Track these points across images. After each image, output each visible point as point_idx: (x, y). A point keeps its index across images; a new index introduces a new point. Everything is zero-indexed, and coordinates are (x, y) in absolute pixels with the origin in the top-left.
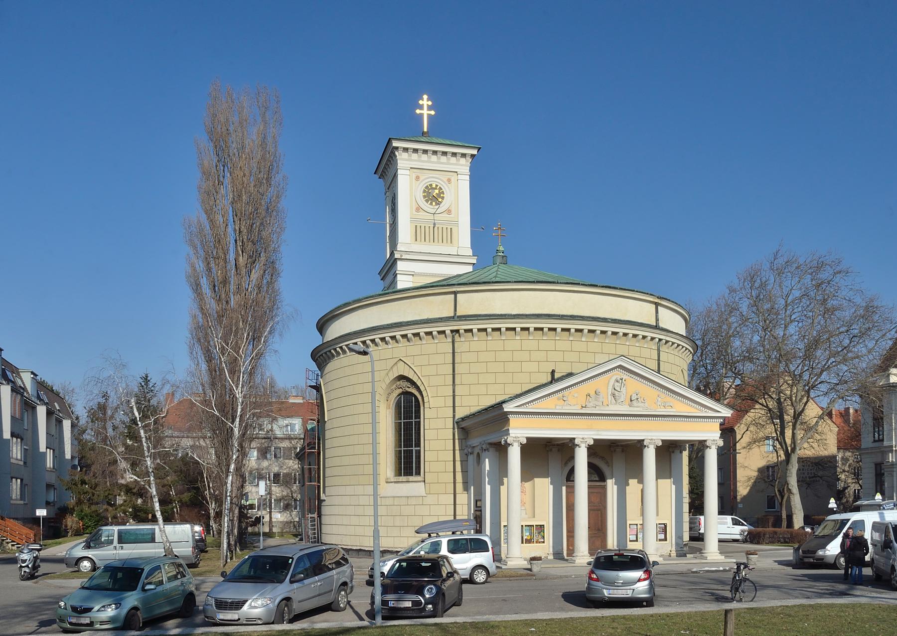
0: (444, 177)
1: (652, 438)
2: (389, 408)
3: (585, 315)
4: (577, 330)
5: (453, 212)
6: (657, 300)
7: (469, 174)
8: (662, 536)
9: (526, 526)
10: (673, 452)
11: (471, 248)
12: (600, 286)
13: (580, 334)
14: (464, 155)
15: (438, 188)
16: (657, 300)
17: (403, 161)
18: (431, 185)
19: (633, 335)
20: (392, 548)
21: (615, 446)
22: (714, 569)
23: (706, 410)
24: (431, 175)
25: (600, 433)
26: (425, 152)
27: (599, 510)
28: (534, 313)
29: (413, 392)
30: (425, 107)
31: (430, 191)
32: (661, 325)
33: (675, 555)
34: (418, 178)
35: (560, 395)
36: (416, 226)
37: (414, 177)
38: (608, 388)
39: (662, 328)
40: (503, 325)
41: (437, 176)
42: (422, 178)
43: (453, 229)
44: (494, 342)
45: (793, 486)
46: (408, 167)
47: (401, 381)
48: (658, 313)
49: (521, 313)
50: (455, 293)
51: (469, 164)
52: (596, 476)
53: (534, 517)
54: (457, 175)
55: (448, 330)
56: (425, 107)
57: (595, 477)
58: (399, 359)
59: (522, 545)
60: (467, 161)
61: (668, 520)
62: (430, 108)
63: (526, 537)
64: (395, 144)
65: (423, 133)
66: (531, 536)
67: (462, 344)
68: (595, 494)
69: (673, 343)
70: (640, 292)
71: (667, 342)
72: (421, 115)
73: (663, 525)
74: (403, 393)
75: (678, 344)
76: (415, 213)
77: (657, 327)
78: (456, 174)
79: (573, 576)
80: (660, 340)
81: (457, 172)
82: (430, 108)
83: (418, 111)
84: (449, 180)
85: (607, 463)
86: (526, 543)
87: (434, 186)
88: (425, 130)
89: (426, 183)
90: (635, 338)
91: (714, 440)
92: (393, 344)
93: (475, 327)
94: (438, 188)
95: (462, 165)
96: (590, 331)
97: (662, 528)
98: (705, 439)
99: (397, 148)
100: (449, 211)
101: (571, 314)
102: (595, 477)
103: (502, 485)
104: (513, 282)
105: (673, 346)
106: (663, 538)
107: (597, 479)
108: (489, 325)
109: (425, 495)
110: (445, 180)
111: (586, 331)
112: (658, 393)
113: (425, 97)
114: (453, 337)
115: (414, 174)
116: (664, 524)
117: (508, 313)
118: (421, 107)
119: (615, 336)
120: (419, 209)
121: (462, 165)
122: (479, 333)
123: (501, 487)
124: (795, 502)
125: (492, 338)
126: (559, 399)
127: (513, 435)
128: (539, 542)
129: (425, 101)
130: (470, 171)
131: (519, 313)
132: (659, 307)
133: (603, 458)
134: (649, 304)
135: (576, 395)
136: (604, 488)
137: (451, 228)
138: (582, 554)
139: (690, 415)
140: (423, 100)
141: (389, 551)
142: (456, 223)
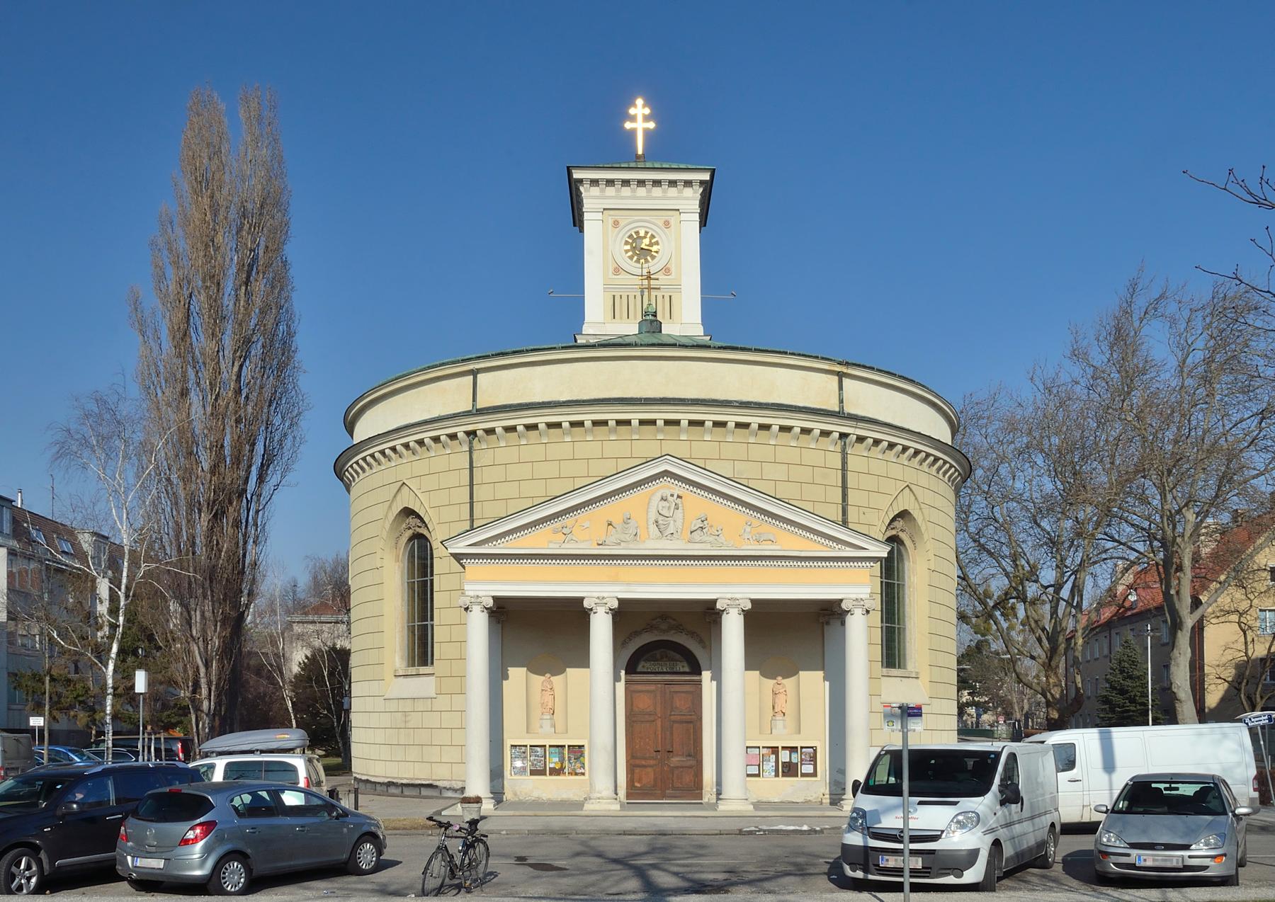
0: (659, 219)
1: (733, 596)
3: (688, 397)
4: (668, 423)
5: (673, 270)
6: (838, 368)
7: (699, 211)
8: (754, 770)
9: (550, 746)
10: (828, 623)
11: (702, 324)
12: (715, 348)
13: (699, 428)
14: (688, 183)
15: (649, 235)
16: (838, 368)
17: (592, 199)
18: (637, 233)
19: (780, 428)
20: (396, 778)
22: (792, 828)
23: (840, 546)
24: (636, 218)
25: (632, 588)
26: (626, 183)
27: (691, 722)
28: (597, 397)
29: (425, 533)
30: (640, 118)
31: (634, 245)
33: (828, 801)
34: (616, 223)
35: (557, 524)
36: (628, 296)
37: (611, 221)
38: (647, 511)
39: (849, 414)
40: (541, 419)
41: (647, 218)
42: (622, 224)
43: (673, 297)
44: (531, 448)
45: (1179, 687)
46: (601, 209)
47: (410, 518)
49: (575, 398)
50: (474, 373)
51: (699, 196)
52: (685, 664)
53: (799, 732)
54: (680, 213)
55: (460, 431)
56: (640, 118)
57: (683, 667)
58: (401, 483)
59: (777, 779)
60: (695, 192)
61: (820, 740)
62: (646, 118)
63: (552, 766)
64: (577, 175)
65: (638, 157)
66: (562, 764)
67: (485, 453)
68: (683, 695)
69: (905, 449)
70: (799, 355)
71: (861, 439)
72: (633, 133)
73: (812, 749)
74: (411, 539)
75: (903, 445)
76: (611, 276)
78: (678, 212)
79: (504, 832)
80: (843, 436)
81: (678, 210)
82: (647, 118)
83: (628, 125)
84: (667, 224)
85: (701, 641)
86: (783, 776)
87: (642, 234)
88: (640, 152)
89: (628, 231)
90: (809, 434)
94: (649, 235)
95: (687, 199)
96: (717, 424)
97: (810, 754)
98: (840, 598)
99: (581, 181)
100: (666, 270)
101: (662, 396)
102: (683, 667)
103: (617, 682)
104: (559, 349)
105: (907, 453)
106: (812, 771)
107: (687, 669)
108: (520, 421)
109: (435, 696)
110: (661, 223)
111: (684, 423)
113: (640, 102)
114: (471, 443)
115: (610, 217)
116: (812, 747)
117: (554, 399)
118: (633, 119)
119: (767, 432)
120: (618, 270)
121: (687, 199)
123: (504, 682)
124: (1183, 715)
125: (549, 439)
126: (555, 532)
127: (472, 594)
128: (576, 774)
129: (640, 109)
130: (699, 207)
131: (571, 399)
132: (843, 379)
133: (692, 634)
134: (824, 375)
135: (587, 524)
136: (699, 683)
137: (670, 297)
138: (599, 795)
139: (803, 554)
140: (635, 106)
141: (393, 782)
142: (677, 287)
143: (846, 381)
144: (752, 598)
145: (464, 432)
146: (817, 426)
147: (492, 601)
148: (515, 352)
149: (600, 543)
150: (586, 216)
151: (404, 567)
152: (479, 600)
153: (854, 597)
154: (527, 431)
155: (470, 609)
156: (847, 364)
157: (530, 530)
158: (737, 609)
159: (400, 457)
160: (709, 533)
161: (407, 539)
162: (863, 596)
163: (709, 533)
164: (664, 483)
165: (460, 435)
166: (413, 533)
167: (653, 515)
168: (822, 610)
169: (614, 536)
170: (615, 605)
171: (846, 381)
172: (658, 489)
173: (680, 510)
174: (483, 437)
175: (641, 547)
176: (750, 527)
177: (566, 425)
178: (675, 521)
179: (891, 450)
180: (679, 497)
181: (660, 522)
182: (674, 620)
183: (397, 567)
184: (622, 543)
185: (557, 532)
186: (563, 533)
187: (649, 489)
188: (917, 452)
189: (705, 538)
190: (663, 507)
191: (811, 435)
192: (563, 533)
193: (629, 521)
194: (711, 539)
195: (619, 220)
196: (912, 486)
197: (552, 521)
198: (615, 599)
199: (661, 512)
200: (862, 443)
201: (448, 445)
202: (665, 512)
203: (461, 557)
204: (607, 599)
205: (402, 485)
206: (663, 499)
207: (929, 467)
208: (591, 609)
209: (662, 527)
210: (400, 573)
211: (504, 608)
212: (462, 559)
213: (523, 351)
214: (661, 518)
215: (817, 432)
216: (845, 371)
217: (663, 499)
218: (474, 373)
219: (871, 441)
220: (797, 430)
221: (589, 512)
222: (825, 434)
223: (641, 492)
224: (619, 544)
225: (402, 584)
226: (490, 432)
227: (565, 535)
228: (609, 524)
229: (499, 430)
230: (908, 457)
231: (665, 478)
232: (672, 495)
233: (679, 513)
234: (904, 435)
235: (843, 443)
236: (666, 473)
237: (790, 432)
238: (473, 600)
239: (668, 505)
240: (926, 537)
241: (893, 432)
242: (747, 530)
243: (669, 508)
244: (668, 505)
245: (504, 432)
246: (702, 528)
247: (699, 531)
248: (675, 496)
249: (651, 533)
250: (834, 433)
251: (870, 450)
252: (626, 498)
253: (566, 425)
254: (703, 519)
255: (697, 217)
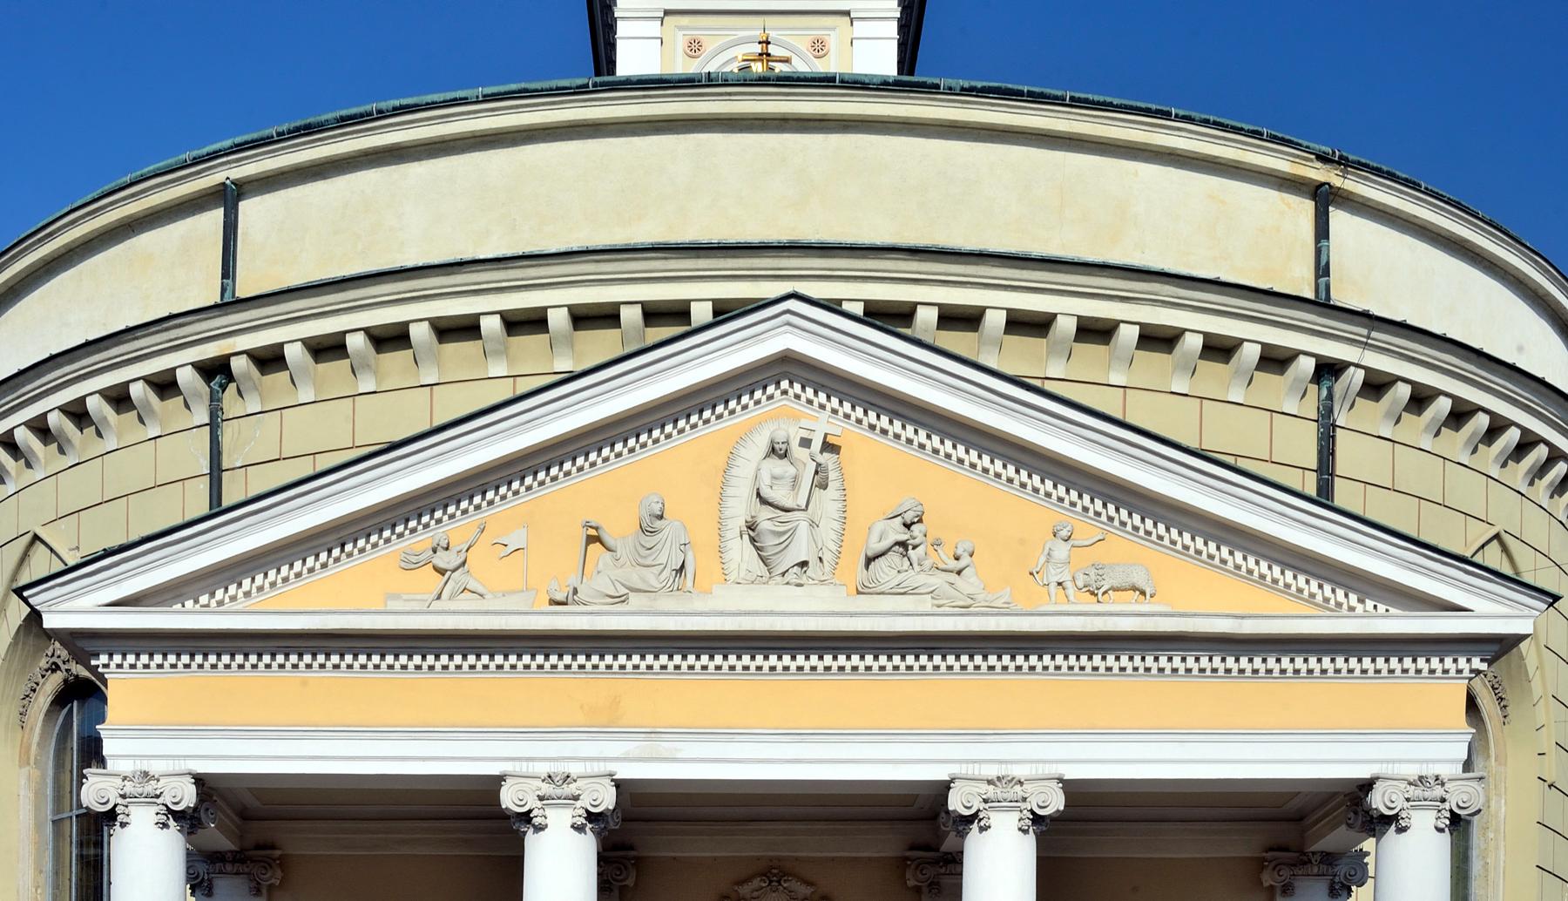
2: (29, 764)
21: (935, 862)
25: (665, 747)
32: (1339, 297)
35: (417, 539)
48: (1327, 237)
55: (182, 363)
58: (28, 537)
71: (1376, 386)
77: (1322, 304)
80: (1328, 370)
81: (847, 13)
91: (1422, 779)
92: (19, 474)
93: (291, 337)
98: (1367, 776)
110: (807, 42)
112: (1053, 515)
122: (322, 367)
126: (410, 565)
127: (126, 767)
132: (1331, 209)
135: (516, 539)
143: (1339, 219)
144: (1074, 773)
145: (195, 365)
146: (1254, 335)
147: (193, 789)
148: (344, 121)
149: (560, 597)
150: (622, 29)
151: (43, 777)
152: (150, 788)
153: (1413, 771)
154: (379, 351)
155: (120, 818)
156: (1343, 163)
157: (323, 556)
158: (1017, 815)
159: (29, 465)
160: (927, 563)
161: (50, 699)
162: (1445, 771)
163: (927, 563)
164: (788, 403)
165: (186, 377)
166: (65, 681)
167: (740, 508)
168: (1271, 849)
169: (604, 573)
170: (606, 799)
171: (1339, 219)
172: (751, 430)
173: (832, 491)
174: (248, 376)
175: (698, 605)
176: (1067, 546)
177: (492, 325)
178: (813, 524)
179: (1457, 430)
180: (828, 447)
181: (764, 525)
182: (808, 883)
183: (23, 782)
184: (631, 595)
185: (418, 566)
186: (436, 569)
187: (728, 422)
188: (1527, 443)
189: (915, 578)
190: (774, 478)
191: (1234, 360)
192: (436, 569)
193: (658, 524)
194: (938, 580)
195: (703, 39)
196: (1507, 539)
197: (399, 529)
198: (607, 781)
199: (766, 492)
200: (1377, 400)
201: (152, 412)
202: (780, 495)
203: (88, 646)
204: (580, 783)
205: (32, 543)
206: (777, 451)
207: (1552, 497)
208: (526, 817)
209: (769, 542)
210: (32, 795)
211: (273, 847)
212: (97, 656)
213: (370, 114)
214: (766, 513)
215: (1251, 353)
216: (1337, 182)
217: (777, 451)
218: (228, 197)
219: (1404, 391)
220: (1193, 343)
221: (525, 498)
222: (1275, 361)
223: (703, 430)
224: (622, 599)
225: (39, 827)
226: (270, 360)
227: (442, 572)
228: (591, 540)
229: (294, 353)
230: (1501, 452)
231: (785, 384)
232: (806, 443)
233: (827, 502)
234: (1498, 382)
235: (1324, 393)
236: (787, 367)
237: (1170, 352)
238: (129, 788)
239: (792, 471)
240: (1537, 687)
241: (1469, 368)
242: (1055, 554)
243: (795, 482)
244: (792, 471)
245: (309, 359)
246: (903, 544)
247: (894, 558)
248: (817, 444)
249: (732, 566)
250: (1302, 358)
251: (1398, 421)
252: (652, 450)
253: (492, 325)
254: (909, 517)
255: (892, 29)
